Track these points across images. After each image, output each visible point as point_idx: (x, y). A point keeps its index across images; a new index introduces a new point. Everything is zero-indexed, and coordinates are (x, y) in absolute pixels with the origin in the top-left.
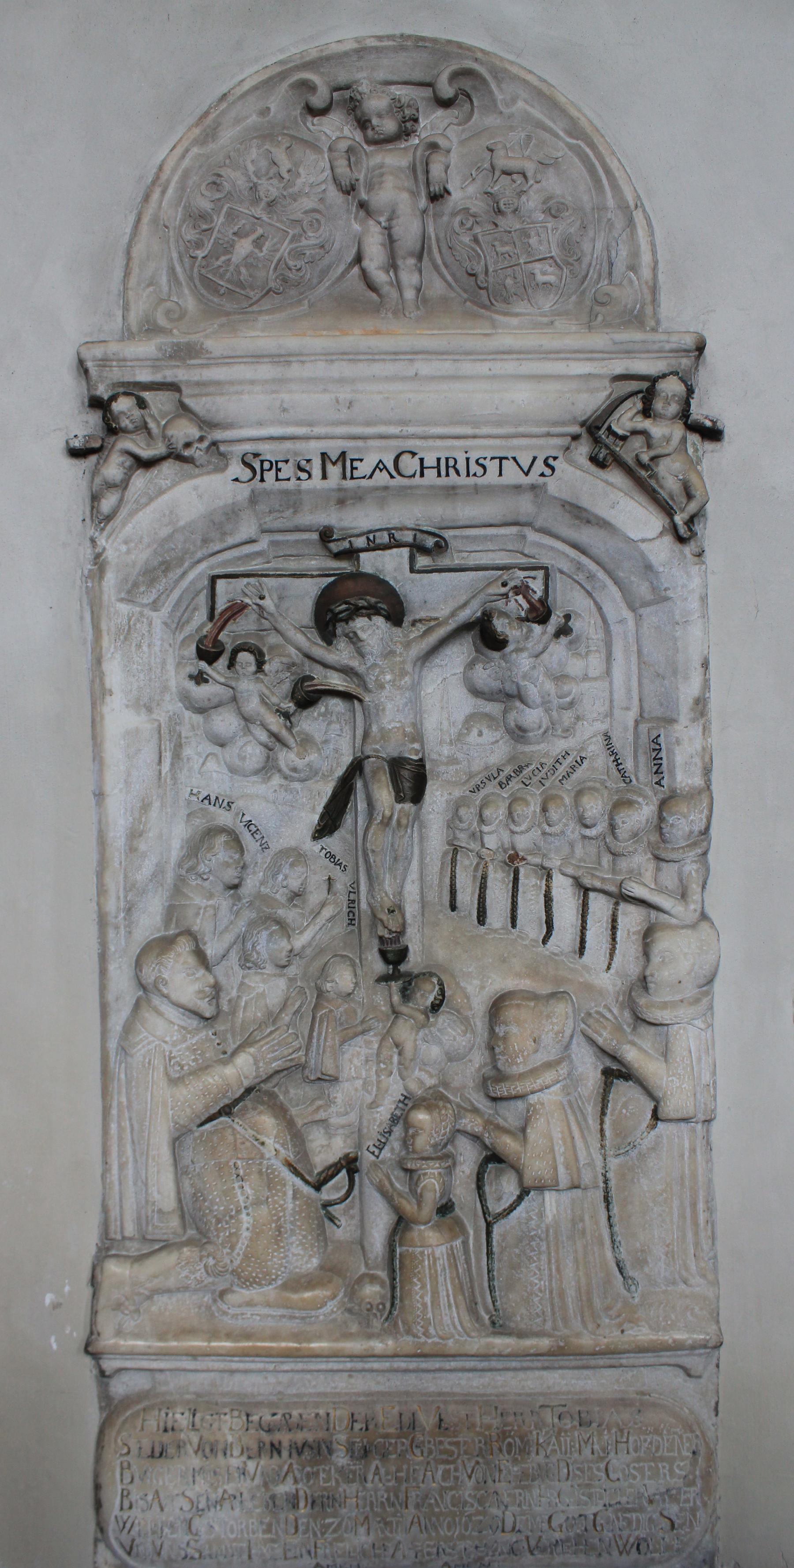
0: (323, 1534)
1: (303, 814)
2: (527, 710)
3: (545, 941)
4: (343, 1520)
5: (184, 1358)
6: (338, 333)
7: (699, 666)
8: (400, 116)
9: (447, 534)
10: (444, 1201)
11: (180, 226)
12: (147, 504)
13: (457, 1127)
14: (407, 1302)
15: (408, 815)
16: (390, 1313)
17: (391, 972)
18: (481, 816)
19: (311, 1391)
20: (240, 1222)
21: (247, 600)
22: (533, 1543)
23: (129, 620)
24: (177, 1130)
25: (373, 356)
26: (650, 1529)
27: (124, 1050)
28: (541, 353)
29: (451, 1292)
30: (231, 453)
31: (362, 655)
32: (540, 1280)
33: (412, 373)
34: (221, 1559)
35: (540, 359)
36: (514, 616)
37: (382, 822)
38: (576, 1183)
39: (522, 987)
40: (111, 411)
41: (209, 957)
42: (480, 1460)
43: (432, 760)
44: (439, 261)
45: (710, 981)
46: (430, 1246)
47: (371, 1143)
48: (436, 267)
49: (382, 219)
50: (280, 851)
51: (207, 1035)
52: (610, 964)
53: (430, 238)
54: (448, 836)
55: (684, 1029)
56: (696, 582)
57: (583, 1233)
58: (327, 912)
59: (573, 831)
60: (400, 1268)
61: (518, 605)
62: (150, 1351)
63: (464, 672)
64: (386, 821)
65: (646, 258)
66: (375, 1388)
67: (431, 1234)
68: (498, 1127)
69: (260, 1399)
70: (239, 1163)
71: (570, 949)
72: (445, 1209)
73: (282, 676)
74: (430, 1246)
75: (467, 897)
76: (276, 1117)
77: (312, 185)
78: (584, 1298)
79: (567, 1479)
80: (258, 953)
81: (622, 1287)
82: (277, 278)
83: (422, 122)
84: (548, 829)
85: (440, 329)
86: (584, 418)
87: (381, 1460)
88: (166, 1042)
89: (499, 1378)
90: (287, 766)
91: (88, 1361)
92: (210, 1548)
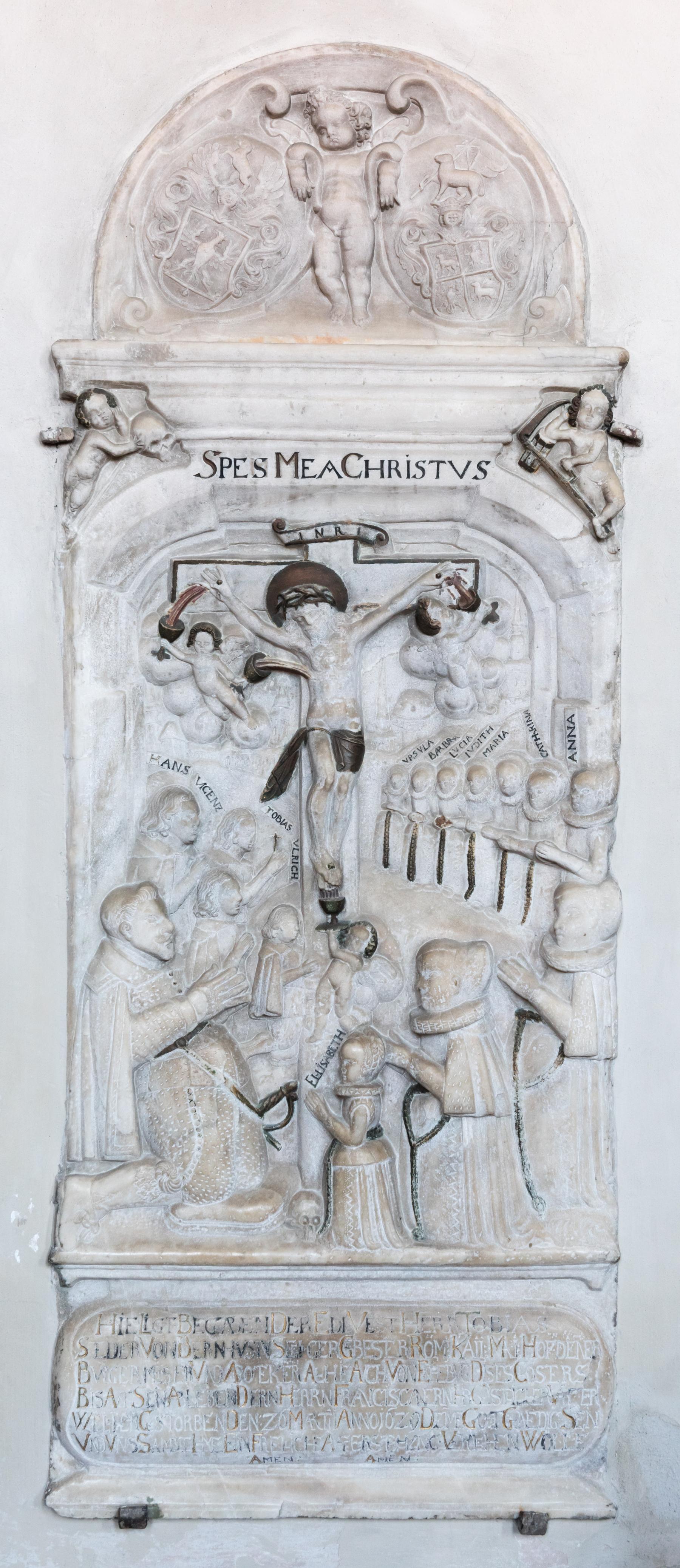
0: (260, 1428)
1: (253, 778)
2: (456, 689)
3: (467, 896)
4: (278, 1415)
5: (139, 1267)
6: (293, 341)
7: (611, 654)
8: (354, 124)
9: (387, 528)
10: (374, 1126)
11: (145, 227)
12: (116, 495)
13: (386, 1060)
14: (339, 1215)
15: (347, 783)
16: (325, 1225)
17: (329, 921)
18: (412, 783)
19: (252, 1298)
20: (192, 1142)
21: (205, 585)
22: (448, 1438)
23: (98, 601)
24: (136, 1060)
25: (326, 365)
26: (554, 1426)
27: (89, 988)
28: (477, 366)
29: (378, 1207)
30: (194, 450)
31: (309, 637)
32: (458, 1198)
33: (359, 381)
34: (168, 1451)
35: (476, 371)
36: (446, 604)
37: (325, 788)
38: (491, 1111)
39: (446, 936)
40: (83, 408)
41: (167, 905)
42: (403, 1360)
43: (370, 732)
44: (388, 269)
45: (614, 934)
46: (361, 1165)
47: (309, 1073)
48: (384, 273)
49: (336, 228)
50: (232, 811)
51: (165, 976)
52: (524, 918)
53: (379, 246)
54: (383, 801)
55: (588, 976)
56: (611, 578)
57: (497, 1156)
58: (274, 866)
59: (495, 799)
60: (334, 1185)
61: (450, 595)
62: (108, 1260)
63: (400, 653)
64: (328, 787)
65: (578, 273)
66: (309, 1295)
67: (362, 1154)
68: (422, 1060)
69: (206, 1305)
70: (192, 1089)
71: (490, 904)
72: (374, 1133)
73: (236, 654)
74: (361, 1165)
75: (399, 856)
76: (226, 1049)
77: (270, 192)
78: (497, 1215)
79: (480, 1379)
80: (211, 903)
81: (531, 1206)
82: (237, 282)
83: (374, 129)
84: (471, 796)
85: (387, 338)
86: (515, 427)
87: (314, 1360)
88: (128, 981)
89: (420, 1287)
90: (240, 735)
91: (50, 1272)
92: (158, 1442)
